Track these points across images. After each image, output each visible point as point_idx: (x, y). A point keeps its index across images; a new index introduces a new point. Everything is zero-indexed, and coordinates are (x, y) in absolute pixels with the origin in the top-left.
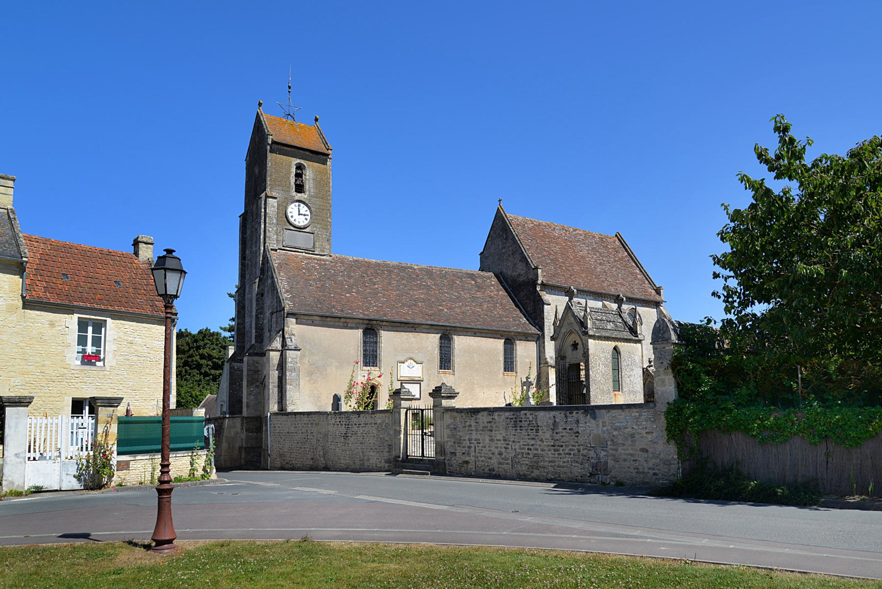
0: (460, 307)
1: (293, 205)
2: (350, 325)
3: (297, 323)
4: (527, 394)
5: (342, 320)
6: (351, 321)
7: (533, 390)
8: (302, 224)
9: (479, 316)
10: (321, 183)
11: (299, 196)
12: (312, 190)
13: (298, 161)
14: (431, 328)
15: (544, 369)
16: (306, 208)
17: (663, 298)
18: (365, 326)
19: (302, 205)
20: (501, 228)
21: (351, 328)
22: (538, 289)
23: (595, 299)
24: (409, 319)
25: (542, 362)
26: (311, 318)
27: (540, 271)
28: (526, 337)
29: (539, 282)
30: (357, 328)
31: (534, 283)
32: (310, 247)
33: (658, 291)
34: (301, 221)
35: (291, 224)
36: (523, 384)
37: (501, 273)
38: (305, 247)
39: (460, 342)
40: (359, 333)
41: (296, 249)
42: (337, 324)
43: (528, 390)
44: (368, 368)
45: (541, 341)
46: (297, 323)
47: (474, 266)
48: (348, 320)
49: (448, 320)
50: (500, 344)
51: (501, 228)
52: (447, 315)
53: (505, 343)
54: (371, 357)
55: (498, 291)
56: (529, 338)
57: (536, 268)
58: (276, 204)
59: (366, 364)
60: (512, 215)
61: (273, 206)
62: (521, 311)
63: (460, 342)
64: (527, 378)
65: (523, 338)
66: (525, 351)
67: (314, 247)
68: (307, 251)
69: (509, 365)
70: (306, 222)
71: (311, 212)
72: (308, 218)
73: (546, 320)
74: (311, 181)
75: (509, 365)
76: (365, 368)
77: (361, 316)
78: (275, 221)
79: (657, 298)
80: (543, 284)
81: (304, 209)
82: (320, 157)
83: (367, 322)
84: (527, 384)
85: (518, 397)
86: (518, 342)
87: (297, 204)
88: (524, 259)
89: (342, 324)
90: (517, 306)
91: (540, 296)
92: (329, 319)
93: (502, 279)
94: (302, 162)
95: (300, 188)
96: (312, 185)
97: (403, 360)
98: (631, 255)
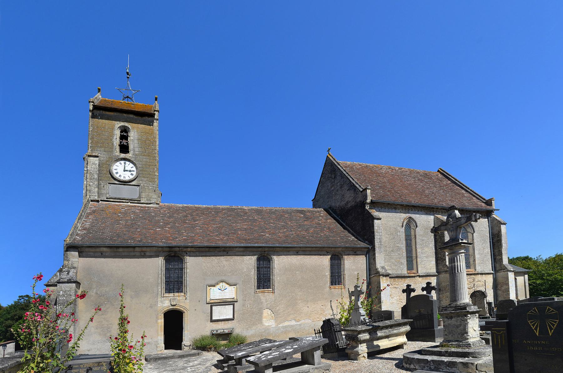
0: (284, 232)
1: (118, 164)
2: (148, 254)
3: (80, 256)
4: (356, 304)
5: (137, 249)
6: (148, 249)
7: (362, 297)
8: (127, 179)
9: (304, 237)
10: (145, 143)
11: (123, 155)
12: (137, 149)
13: (122, 124)
14: (246, 251)
15: (374, 279)
16: (131, 165)
17: (494, 207)
18: (166, 254)
19: (127, 163)
20: (331, 170)
21: (150, 257)
22: (367, 207)
23: (427, 214)
24: (220, 244)
25: (372, 272)
26: (98, 250)
27: (369, 191)
28: (355, 252)
29: (369, 201)
30: (157, 256)
31: (363, 203)
32: (136, 197)
33: (489, 203)
34: (127, 176)
35: (115, 179)
36: (351, 294)
37: (330, 208)
38: (130, 198)
39: (279, 262)
40: (160, 262)
41: (120, 200)
42: (132, 254)
43: (357, 300)
44: (172, 295)
45: (371, 253)
46: (80, 256)
47: (308, 206)
48: (144, 249)
49: (266, 243)
50: (325, 260)
51: (331, 170)
52: (267, 238)
53: (331, 259)
54: (174, 283)
55: (327, 220)
56: (358, 253)
57: (365, 189)
58: (97, 162)
59: (169, 290)
60: (343, 162)
61: (93, 164)
62: (349, 232)
63: (279, 262)
64: (356, 287)
65: (351, 252)
66: (355, 266)
67: (140, 197)
68: (131, 200)
69: (336, 278)
70: (132, 177)
71: (137, 168)
72: (135, 173)
73: (376, 234)
74: (136, 141)
75: (336, 278)
76: (167, 295)
77: (161, 244)
78: (96, 176)
79: (489, 208)
80: (373, 204)
81: (129, 166)
82: (145, 117)
83: (168, 249)
84: (356, 293)
85: (346, 307)
86: (345, 257)
87: (122, 162)
88: (353, 187)
89: (138, 254)
90: (345, 228)
91: (370, 213)
92: (121, 250)
93: (331, 211)
94: (126, 124)
95: (124, 149)
96: (136, 145)
97: (213, 282)
98: (455, 182)
